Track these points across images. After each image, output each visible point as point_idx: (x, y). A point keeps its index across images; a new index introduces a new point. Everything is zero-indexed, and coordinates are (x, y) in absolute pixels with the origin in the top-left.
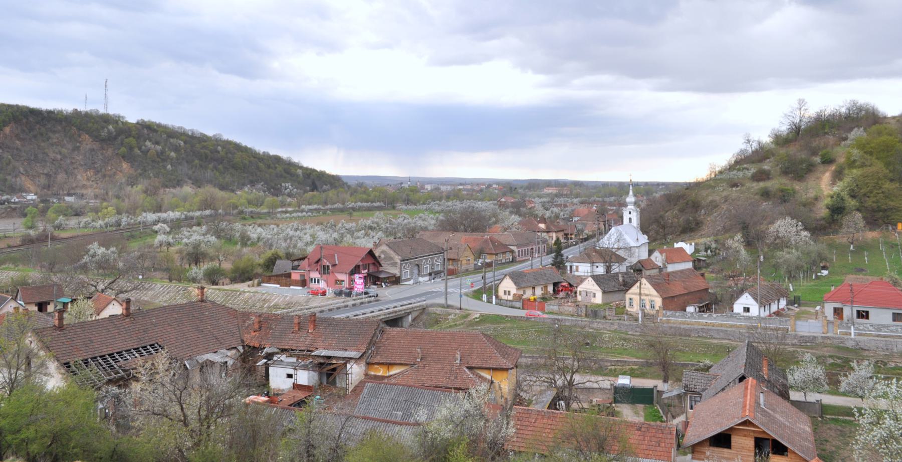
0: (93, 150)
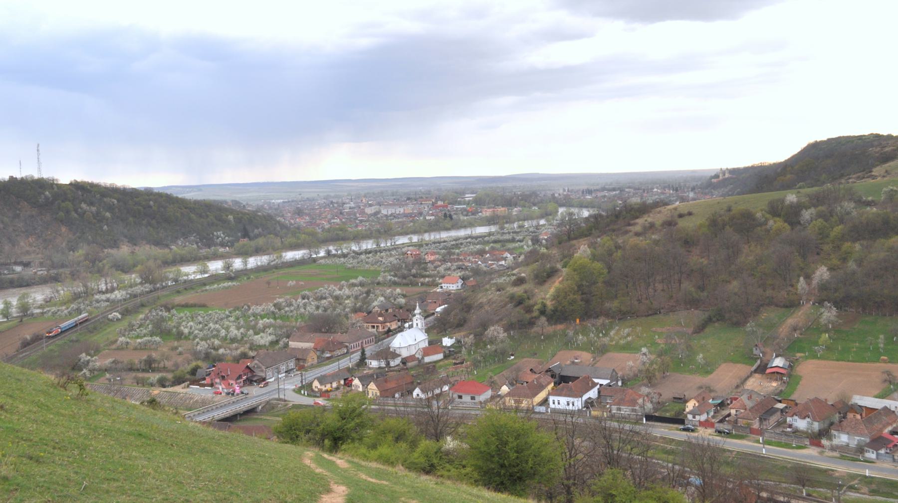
0: (33, 216)
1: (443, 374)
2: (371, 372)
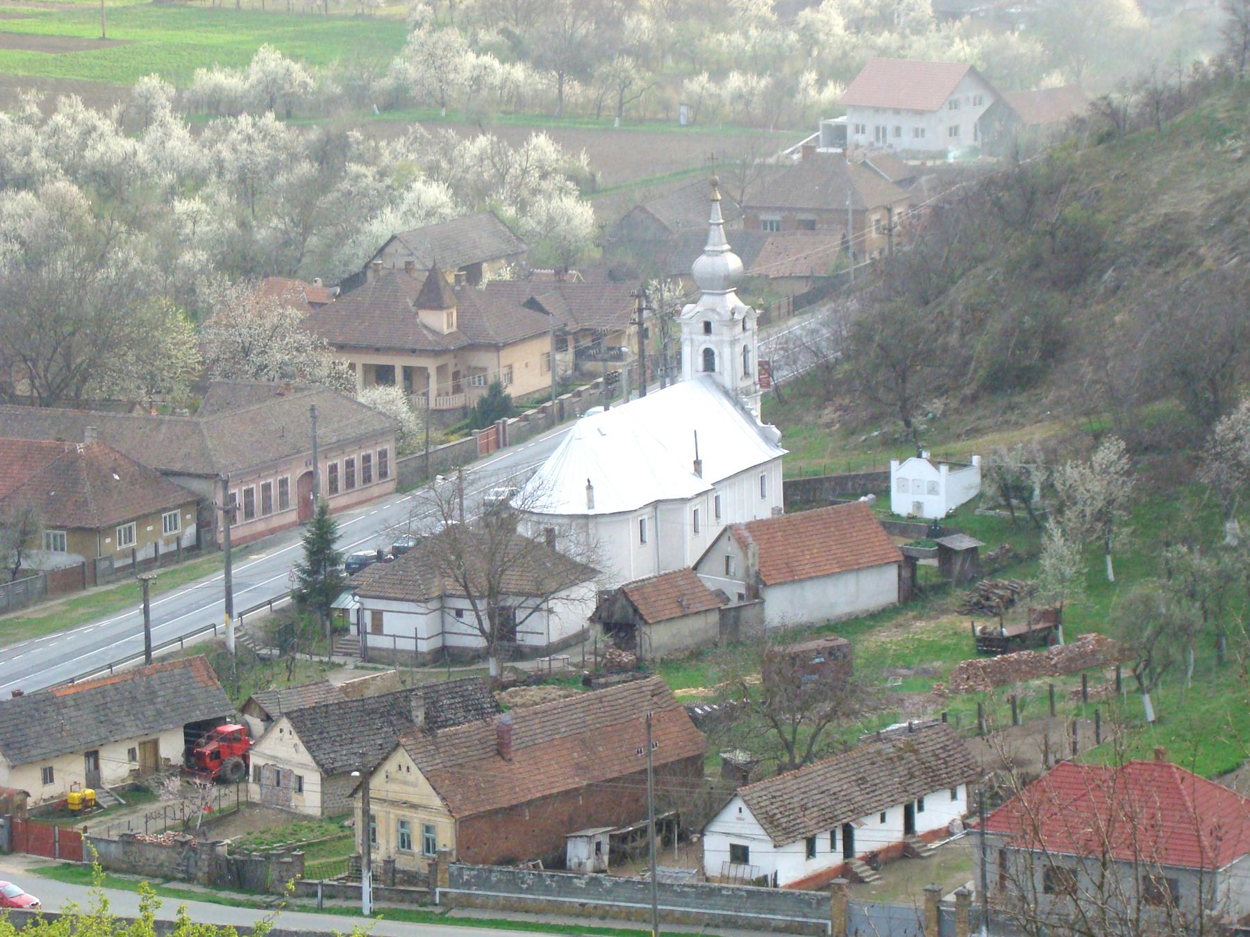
1: (911, 717)
2: (382, 679)
